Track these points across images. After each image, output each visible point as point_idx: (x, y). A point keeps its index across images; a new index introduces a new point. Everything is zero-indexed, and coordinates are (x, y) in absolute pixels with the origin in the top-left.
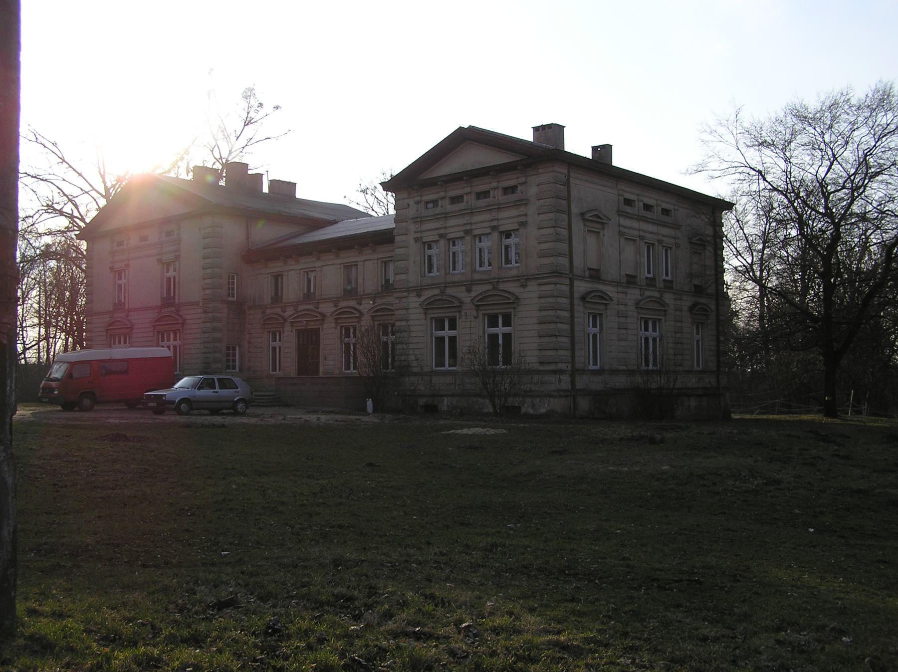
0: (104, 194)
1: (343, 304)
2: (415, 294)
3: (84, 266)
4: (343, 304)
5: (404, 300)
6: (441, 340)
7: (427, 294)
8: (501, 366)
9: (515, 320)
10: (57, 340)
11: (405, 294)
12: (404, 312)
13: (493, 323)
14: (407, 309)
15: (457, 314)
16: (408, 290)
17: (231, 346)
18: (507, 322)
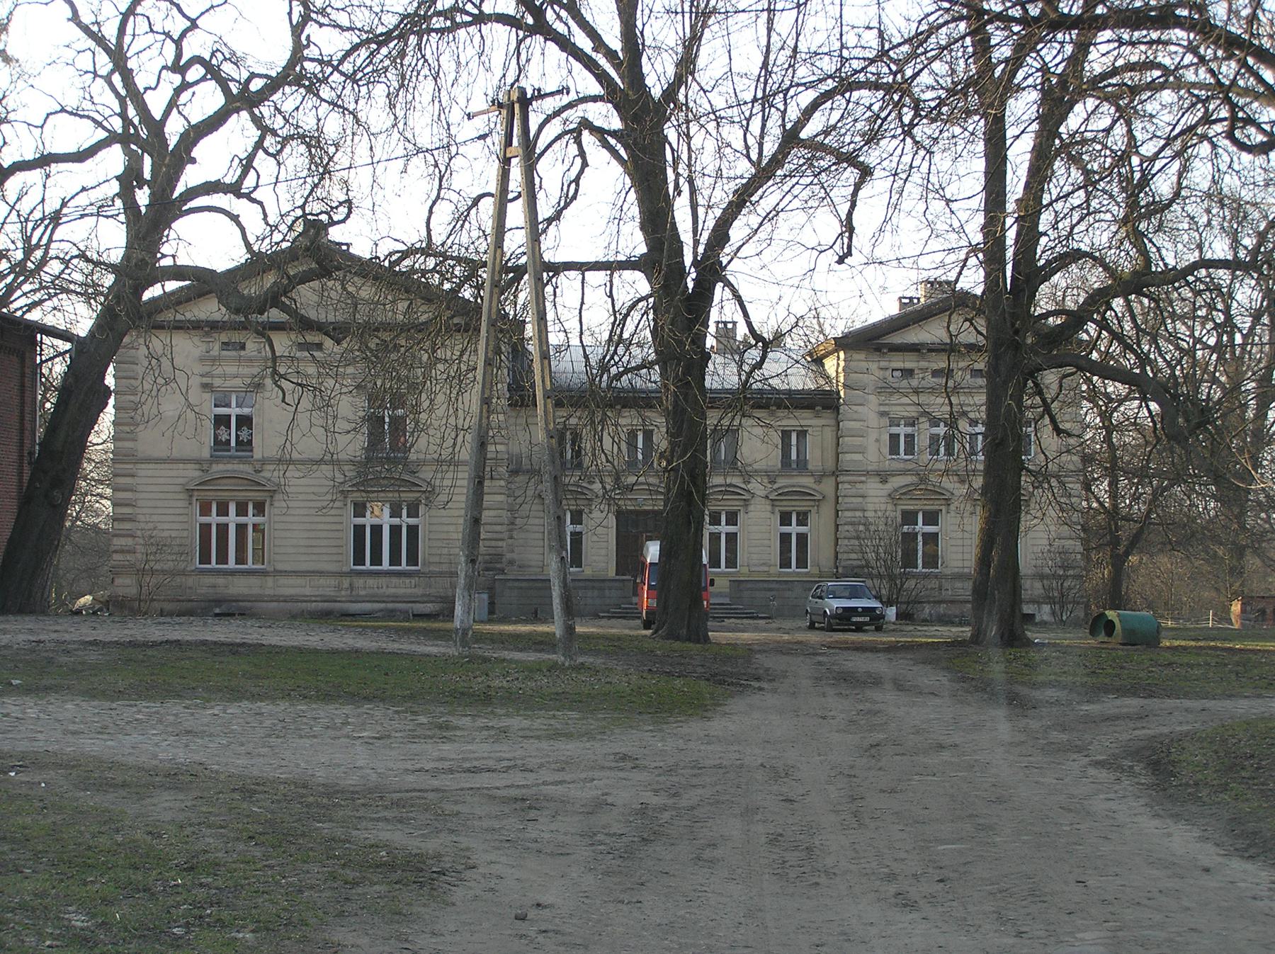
0: (175, 109)
1: (782, 482)
2: (878, 479)
3: (1057, 141)
4: (782, 482)
5: (858, 486)
6: (785, 538)
7: (897, 482)
8: (250, 565)
9: (811, 519)
10: (743, 117)
11: (863, 479)
12: (860, 500)
13: (205, 511)
14: (863, 497)
15: (943, 508)
16: (867, 473)
17: (368, 566)
18: (413, 513)
